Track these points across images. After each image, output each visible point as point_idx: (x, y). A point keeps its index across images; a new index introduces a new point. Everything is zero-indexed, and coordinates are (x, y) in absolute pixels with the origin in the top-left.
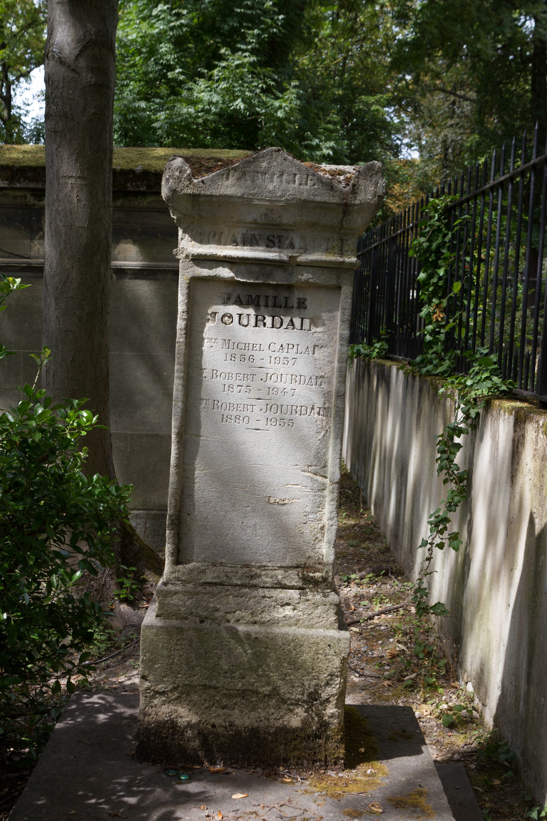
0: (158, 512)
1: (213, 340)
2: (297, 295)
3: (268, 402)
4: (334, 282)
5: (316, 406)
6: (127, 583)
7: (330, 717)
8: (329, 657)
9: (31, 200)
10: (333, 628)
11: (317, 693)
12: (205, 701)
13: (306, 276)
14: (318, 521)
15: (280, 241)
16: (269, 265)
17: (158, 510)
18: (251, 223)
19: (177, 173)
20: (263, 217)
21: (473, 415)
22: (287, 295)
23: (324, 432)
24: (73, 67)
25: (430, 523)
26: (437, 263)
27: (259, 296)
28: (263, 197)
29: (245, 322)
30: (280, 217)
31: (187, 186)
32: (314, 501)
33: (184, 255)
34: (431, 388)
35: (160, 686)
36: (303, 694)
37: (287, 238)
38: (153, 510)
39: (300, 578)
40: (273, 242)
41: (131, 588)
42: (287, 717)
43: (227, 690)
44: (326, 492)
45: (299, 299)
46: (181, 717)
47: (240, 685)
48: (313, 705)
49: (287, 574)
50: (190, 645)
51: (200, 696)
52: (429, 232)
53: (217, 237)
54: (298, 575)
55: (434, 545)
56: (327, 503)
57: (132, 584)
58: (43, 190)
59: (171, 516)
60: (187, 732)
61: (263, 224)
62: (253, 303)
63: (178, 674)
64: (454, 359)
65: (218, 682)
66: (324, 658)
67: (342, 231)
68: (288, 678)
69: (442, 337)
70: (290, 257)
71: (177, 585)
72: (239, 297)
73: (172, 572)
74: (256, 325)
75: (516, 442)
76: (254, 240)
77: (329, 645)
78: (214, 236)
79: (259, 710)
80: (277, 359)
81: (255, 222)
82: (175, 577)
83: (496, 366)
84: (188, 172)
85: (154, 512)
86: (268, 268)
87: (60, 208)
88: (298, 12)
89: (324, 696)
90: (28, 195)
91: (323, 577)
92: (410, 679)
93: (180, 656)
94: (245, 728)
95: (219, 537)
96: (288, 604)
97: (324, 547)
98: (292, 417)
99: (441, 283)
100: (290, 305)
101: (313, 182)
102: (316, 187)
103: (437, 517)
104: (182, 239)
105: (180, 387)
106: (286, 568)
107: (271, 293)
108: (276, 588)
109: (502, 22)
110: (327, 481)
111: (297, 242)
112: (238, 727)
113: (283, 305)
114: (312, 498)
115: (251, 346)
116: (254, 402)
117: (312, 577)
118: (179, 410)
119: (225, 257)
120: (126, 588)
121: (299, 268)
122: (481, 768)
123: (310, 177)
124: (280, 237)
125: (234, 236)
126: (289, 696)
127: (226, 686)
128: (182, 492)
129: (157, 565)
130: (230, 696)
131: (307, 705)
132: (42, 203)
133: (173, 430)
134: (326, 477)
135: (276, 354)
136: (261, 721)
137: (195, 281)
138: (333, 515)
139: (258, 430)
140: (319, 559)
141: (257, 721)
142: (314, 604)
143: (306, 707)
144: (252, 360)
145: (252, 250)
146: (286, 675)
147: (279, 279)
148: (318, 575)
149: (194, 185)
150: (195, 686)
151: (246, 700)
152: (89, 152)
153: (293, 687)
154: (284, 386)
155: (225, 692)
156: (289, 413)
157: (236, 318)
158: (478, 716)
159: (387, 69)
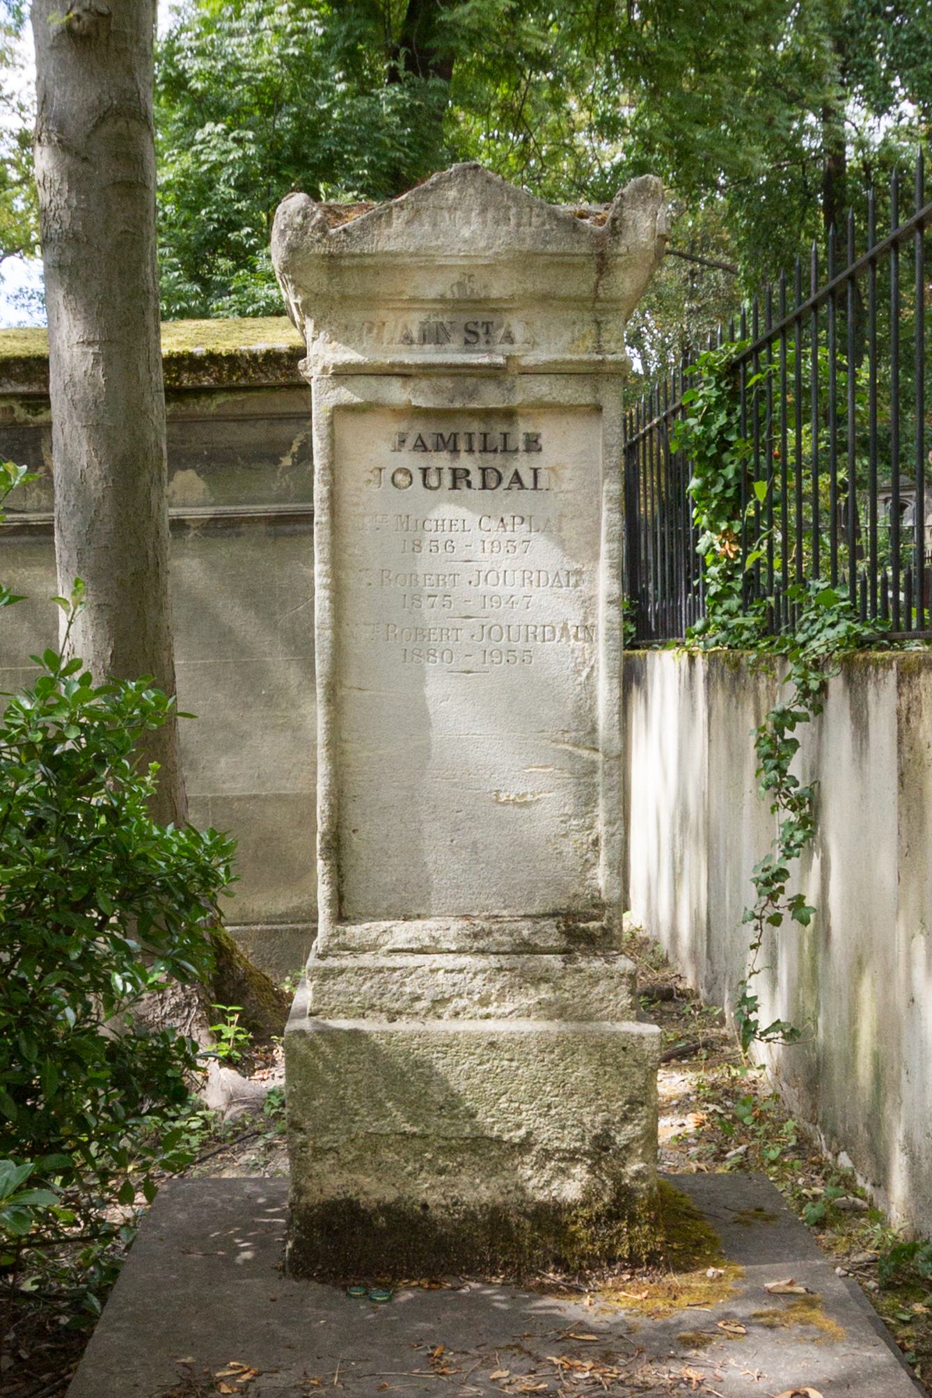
0: (265, 927)
1: (379, 518)
2: (523, 427)
3: (484, 621)
4: (588, 399)
5: (570, 623)
6: (229, 1032)
7: (632, 1179)
8: (626, 1069)
9: (21, 413)
10: (628, 1019)
11: (608, 1136)
12: (407, 1161)
13: (542, 389)
14: (588, 829)
15: (487, 332)
16: (471, 375)
17: (267, 923)
18: (435, 301)
19: (299, 219)
20: (455, 288)
21: (814, 685)
22: (506, 430)
23: (588, 669)
24: (83, 155)
25: (756, 881)
26: (721, 460)
27: (455, 435)
28: (455, 252)
29: (433, 481)
30: (485, 287)
31: (319, 241)
32: (578, 794)
33: (319, 368)
34: (727, 669)
35: (325, 1139)
36: (583, 1139)
37: (500, 326)
38: (257, 924)
40: (476, 334)
41: (236, 1040)
42: (555, 1184)
43: (446, 1139)
44: (599, 778)
45: (527, 435)
46: (365, 1193)
47: (468, 1130)
48: (600, 1158)
49: (538, 927)
50: (374, 1062)
51: (398, 1154)
52: (702, 408)
53: (375, 331)
54: (558, 927)
55: (764, 920)
56: (600, 797)
57: (238, 1032)
58: (46, 396)
59: (324, 835)
60: (377, 1219)
61: (458, 301)
62: (446, 447)
63: (356, 1115)
64: (763, 615)
65: (428, 1127)
66: (615, 1072)
67: (598, 305)
68: (553, 1112)
69: (738, 586)
71: (342, 956)
72: (420, 437)
73: (333, 935)
74: (454, 487)
75: (904, 713)
77: (624, 1049)
78: (370, 330)
79: (504, 1173)
80: (496, 544)
81: (442, 300)
82: (338, 944)
83: (848, 603)
84: (318, 216)
85: (259, 927)
86: (470, 382)
87: (77, 397)
88: (434, 123)
89: (620, 1140)
90: (16, 407)
91: (602, 928)
92: (736, 1155)
93: (356, 1083)
94: (481, 1206)
95: (411, 869)
96: (547, 981)
97: (600, 875)
98: (528, 646)
99: (730, 493)
100: (511, 446)
101: (541, 219)
102: (547, 227)
103: (765, 870)
104: (314, 339)
105: (327, 603)
106: (535, 918)
107: (476, 427)
108: (522, 953)
109: (771, 120)
110: (599, 757)
111: (519, 332)
112: (468, 1206)
113: (500, 448)
114: (574, 790)
115: (447, 523)
116: (458, 623)
117: (584, 930)
118: (327, 644)
119: (392, 365)
120: (228, 1040)
121: (525, 378)
122: (888, 1287)
123: (536, 211)
124: (487, 325)
125: (405, 327)
126: (556, 1144)
127: (443, 1133)
128: (341, 791)
129: (276, 1002)
130: (450, 1151)
131: (592, 1158)
132: (41, 418)
133: (318, 680)
134: (597, 750)
135: (494, 536)
136: (509, 1192)
137: (342, 410)
138: (613, 816)
139: (469, 672)
140: (593, 897)
141: (502, 1193)
142: (591, 976)
143: (589, 1162)
146: (549, 1106)
147: (491, 397)
148: (593, 925)
149: (330, 239)
150: (387, 1135)
151: (481, 1155)
152: (119, 299)
153: (563, 1128)
154: (509, 590)
155: (444, 1143)
156: (522, 639)
157: (418, 477)
158: (866, 1205)
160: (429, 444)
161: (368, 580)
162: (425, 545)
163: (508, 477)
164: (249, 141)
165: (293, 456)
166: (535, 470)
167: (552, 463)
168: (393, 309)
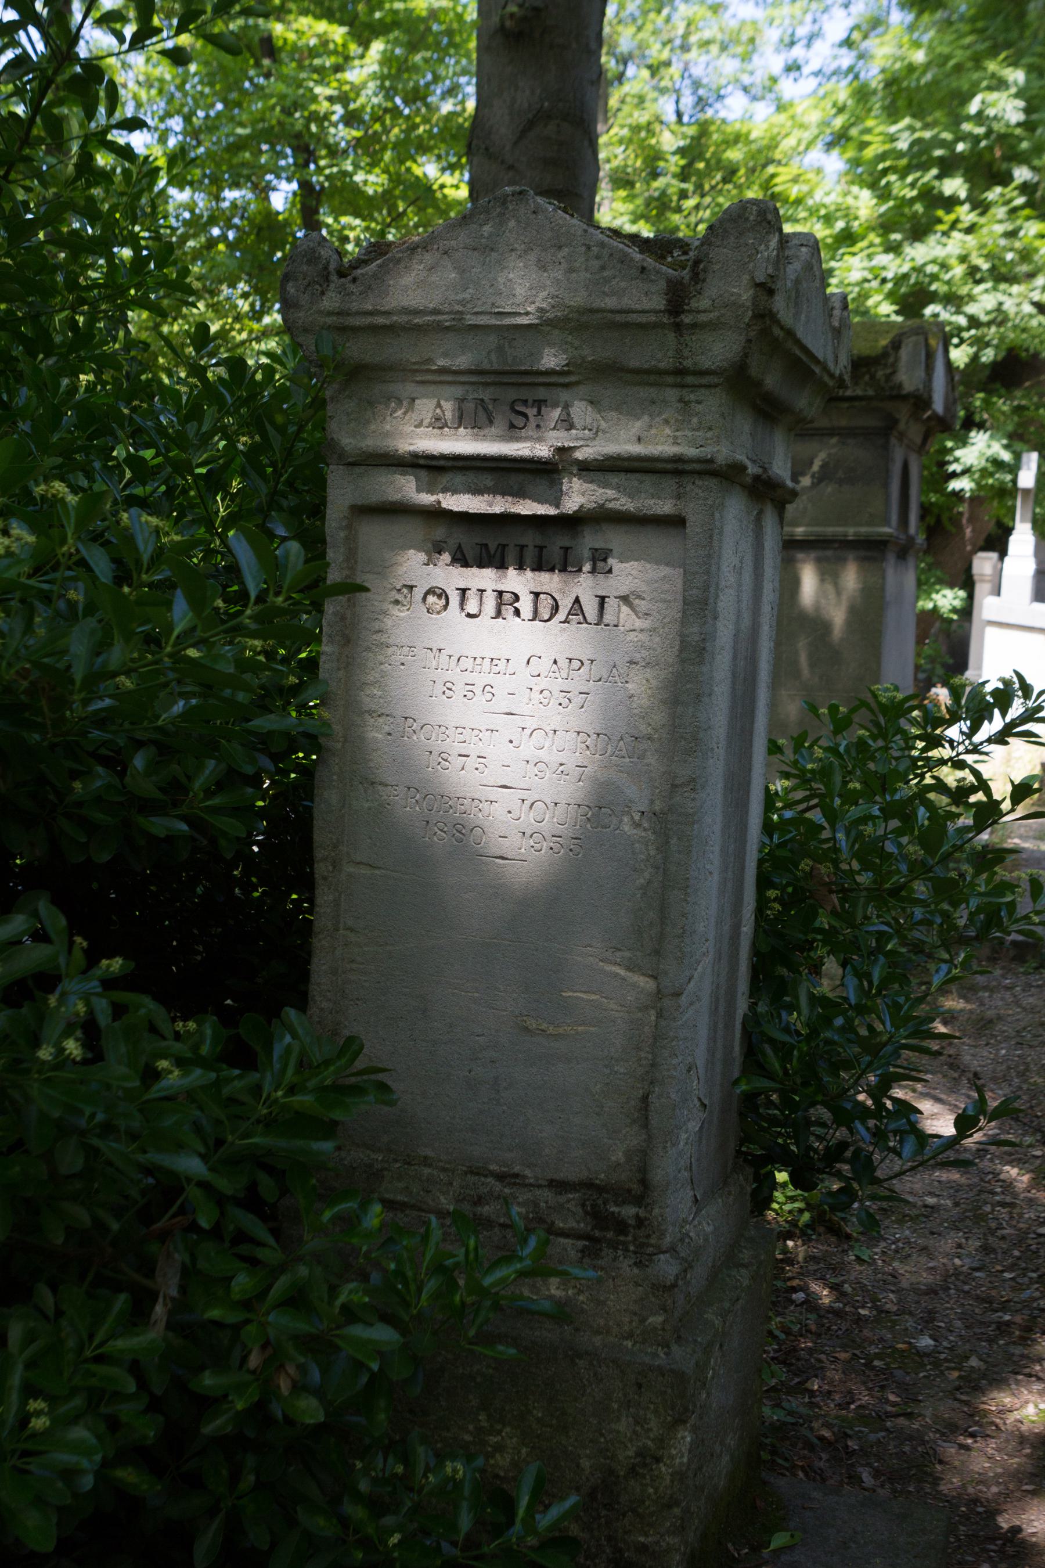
3: (525, 794)
18: (470, 372)
20: (493, 357)
22: (567, 544)
28: (487, 308)
29: (472, 607)
39: (586, 1213)
54: (583, 1205)
70: (561, 450)
72: (460, 546)
76: (481, 413)
117: (613, 1213)
144: (489, 696)
145: (476, 438)
159: (431, 39)
160: (469, 557)
161: (387, 729)
162: (459, 689)
163: (565, 605)
164: (394, 188)
165: (813, 476)
166: (602, 600)
167: (624, 591)
168: (423, 382)
